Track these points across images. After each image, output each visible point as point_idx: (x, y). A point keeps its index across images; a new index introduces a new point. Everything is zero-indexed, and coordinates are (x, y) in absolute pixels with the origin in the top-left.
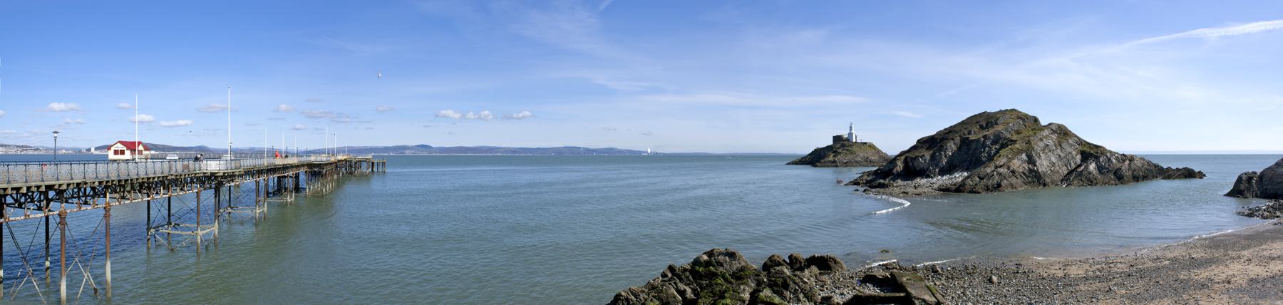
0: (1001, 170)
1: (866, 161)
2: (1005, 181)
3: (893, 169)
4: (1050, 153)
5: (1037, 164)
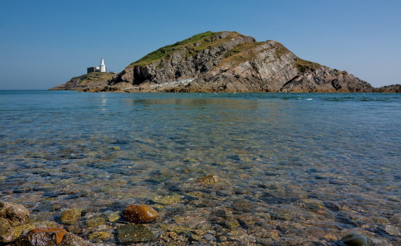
0: (226, 74)
2: (230, 84)
4: (270, 63)
5: (260, 71)
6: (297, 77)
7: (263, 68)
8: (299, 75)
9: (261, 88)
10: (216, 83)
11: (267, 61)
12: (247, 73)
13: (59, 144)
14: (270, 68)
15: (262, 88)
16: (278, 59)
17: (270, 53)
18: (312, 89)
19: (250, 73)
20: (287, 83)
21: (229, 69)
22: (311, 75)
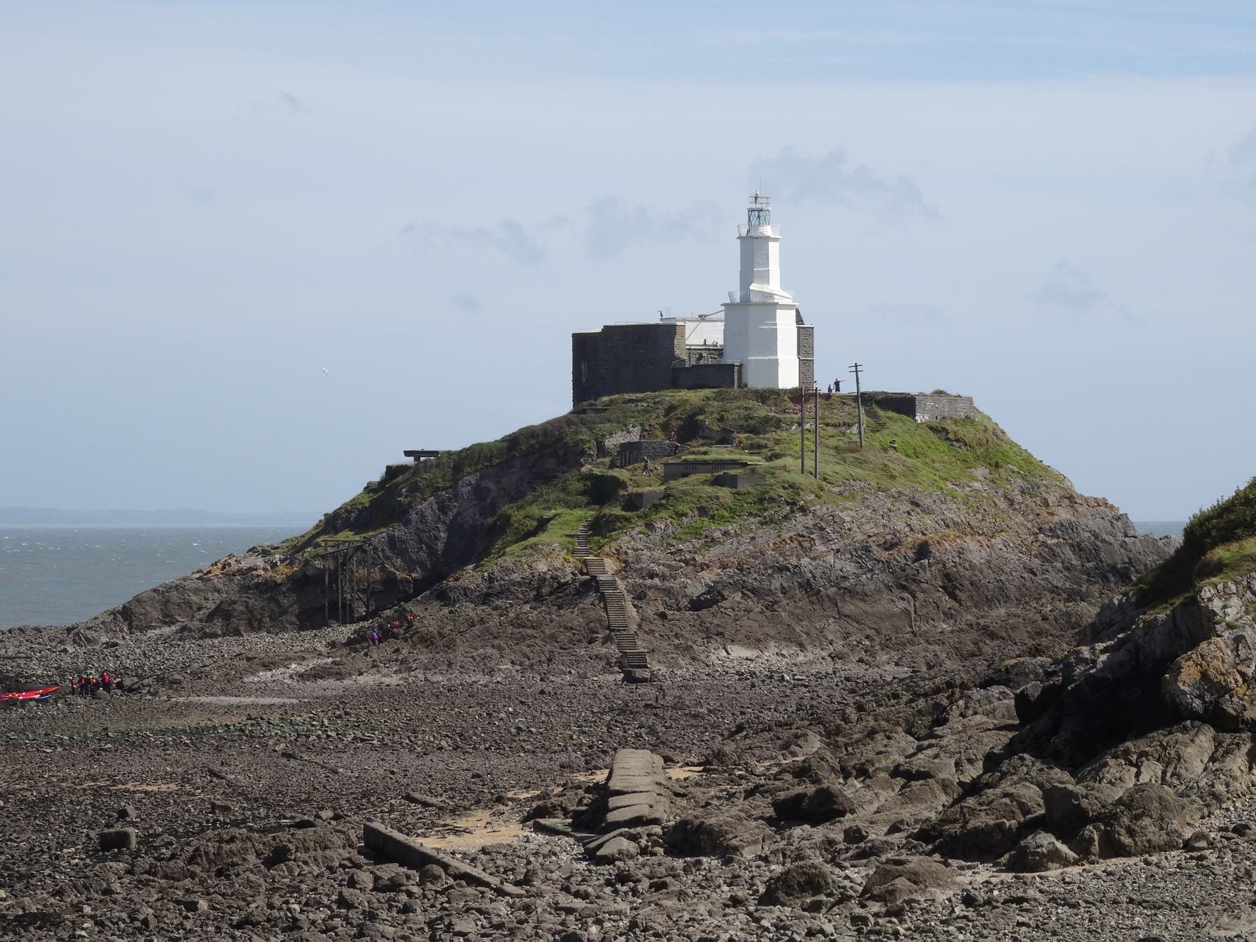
1: (905, 583)
3: (1169, 662)
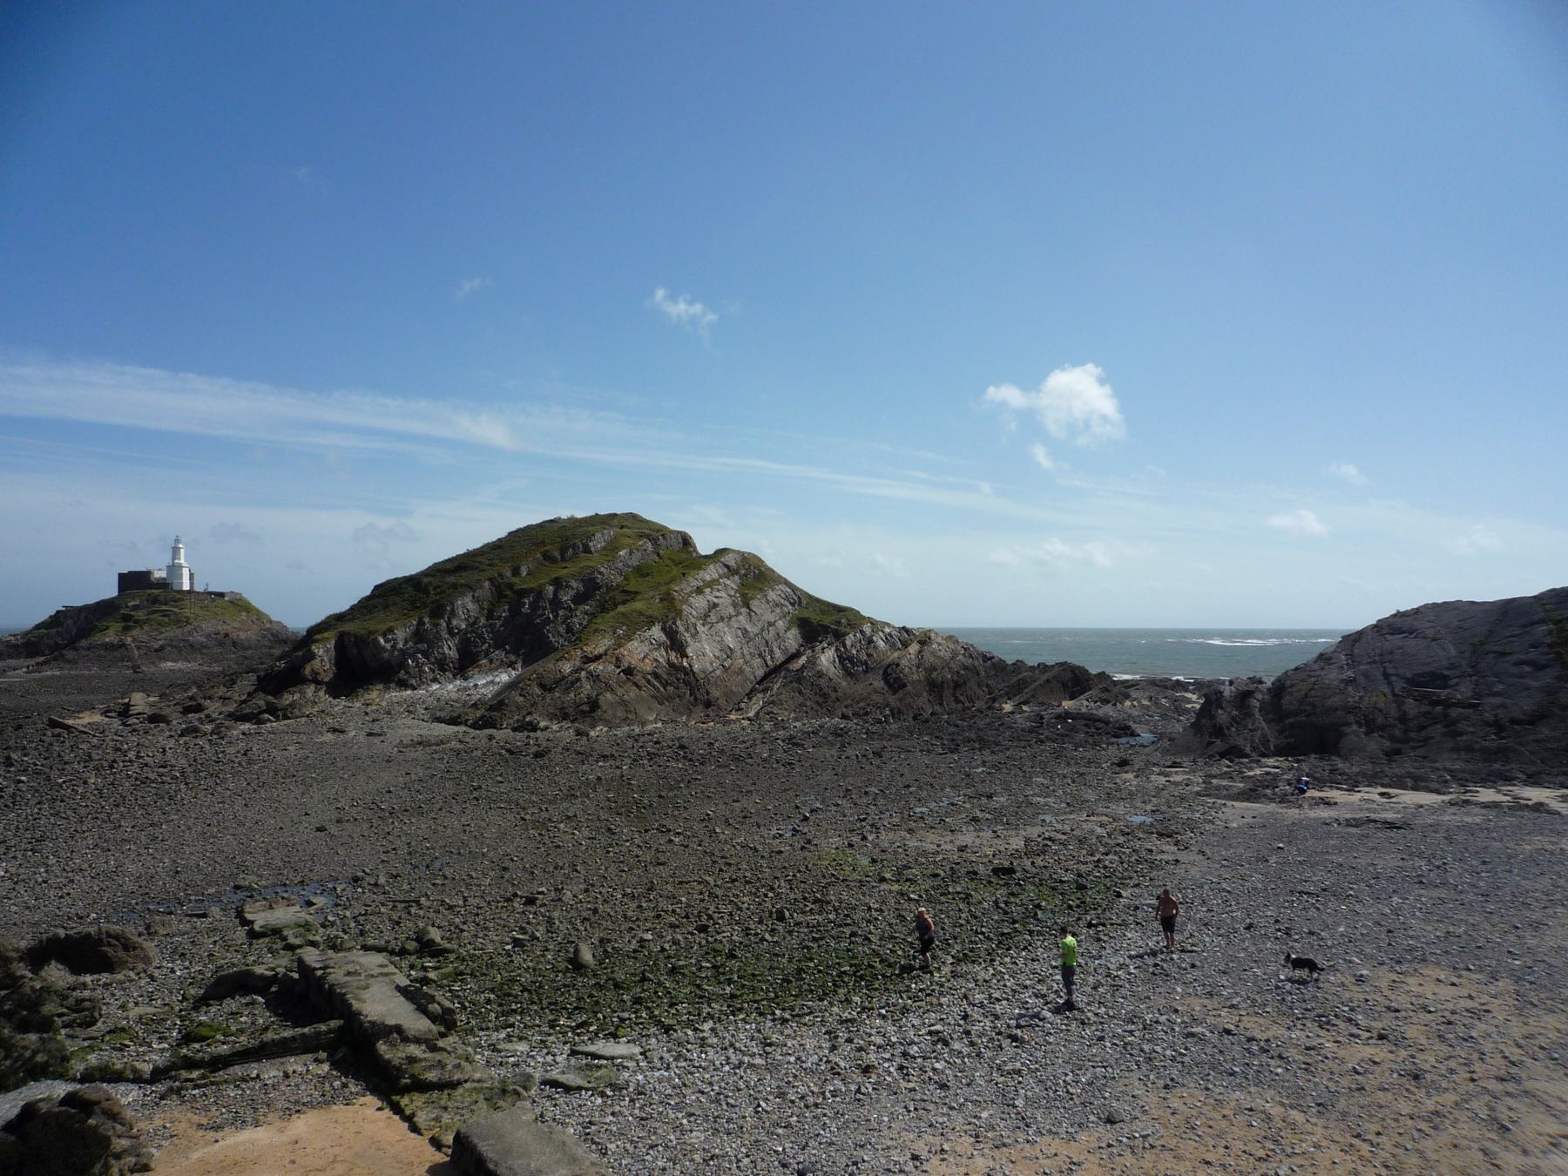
2: (609, 695)
5: (689, 651)
6: (796, 656)
7: (700, 642)
8: (802, 649)
9: (692, 698)
10: (572, 695)
11: (713, 618)
12: (656, 660)
13: (1346, 1009)
14: (719, 639)
15: (696, 699)
16: (744, 610)
17: (723, 594)
18: (825, 696)
19: (663, 657)
20: (766, 677)
21: (606, 654)
22: (833, 649)
